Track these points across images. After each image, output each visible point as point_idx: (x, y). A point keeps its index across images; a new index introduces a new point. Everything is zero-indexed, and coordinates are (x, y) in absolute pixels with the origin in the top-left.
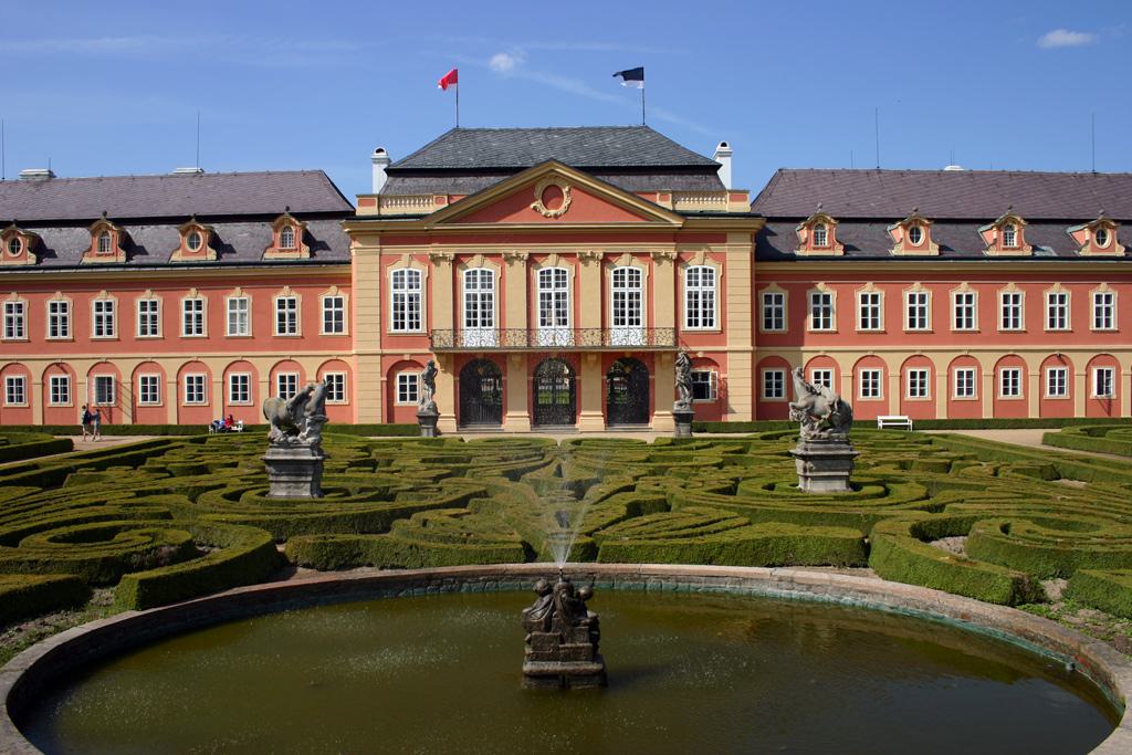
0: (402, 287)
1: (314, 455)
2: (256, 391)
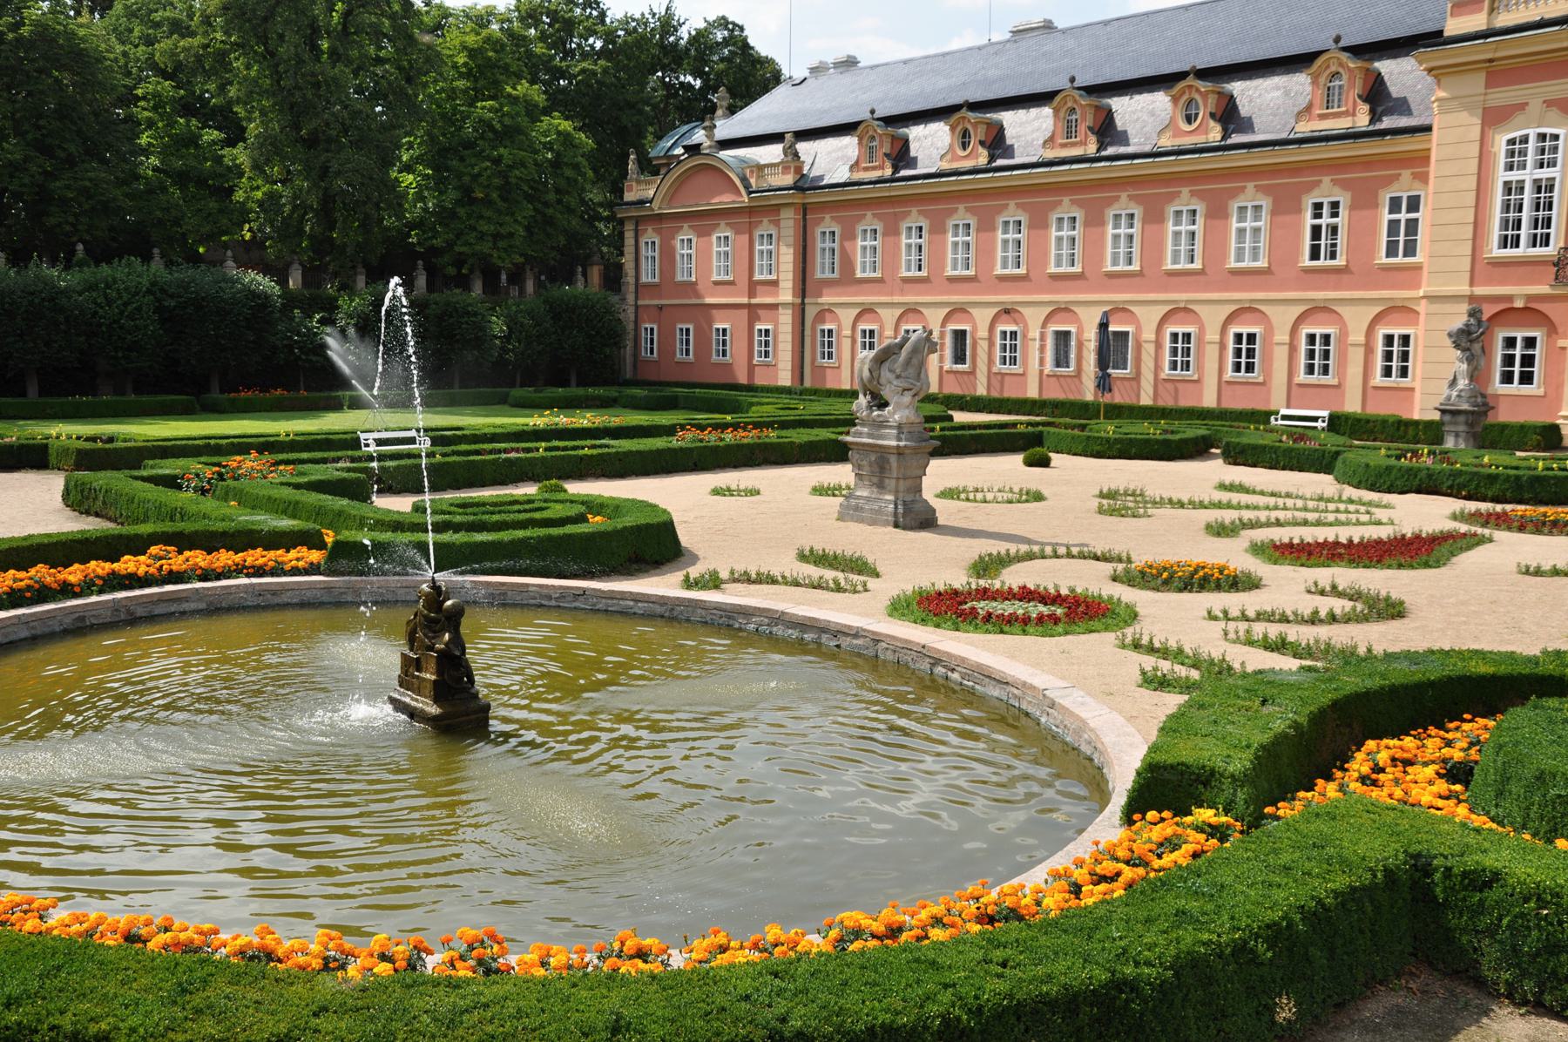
0: (1523, 166)
1: (899, 439)
2: (1268, 359)
